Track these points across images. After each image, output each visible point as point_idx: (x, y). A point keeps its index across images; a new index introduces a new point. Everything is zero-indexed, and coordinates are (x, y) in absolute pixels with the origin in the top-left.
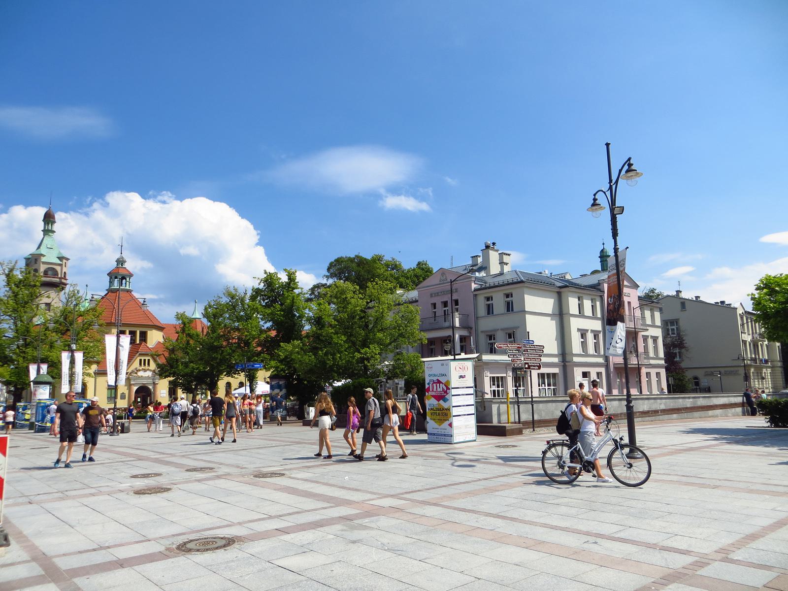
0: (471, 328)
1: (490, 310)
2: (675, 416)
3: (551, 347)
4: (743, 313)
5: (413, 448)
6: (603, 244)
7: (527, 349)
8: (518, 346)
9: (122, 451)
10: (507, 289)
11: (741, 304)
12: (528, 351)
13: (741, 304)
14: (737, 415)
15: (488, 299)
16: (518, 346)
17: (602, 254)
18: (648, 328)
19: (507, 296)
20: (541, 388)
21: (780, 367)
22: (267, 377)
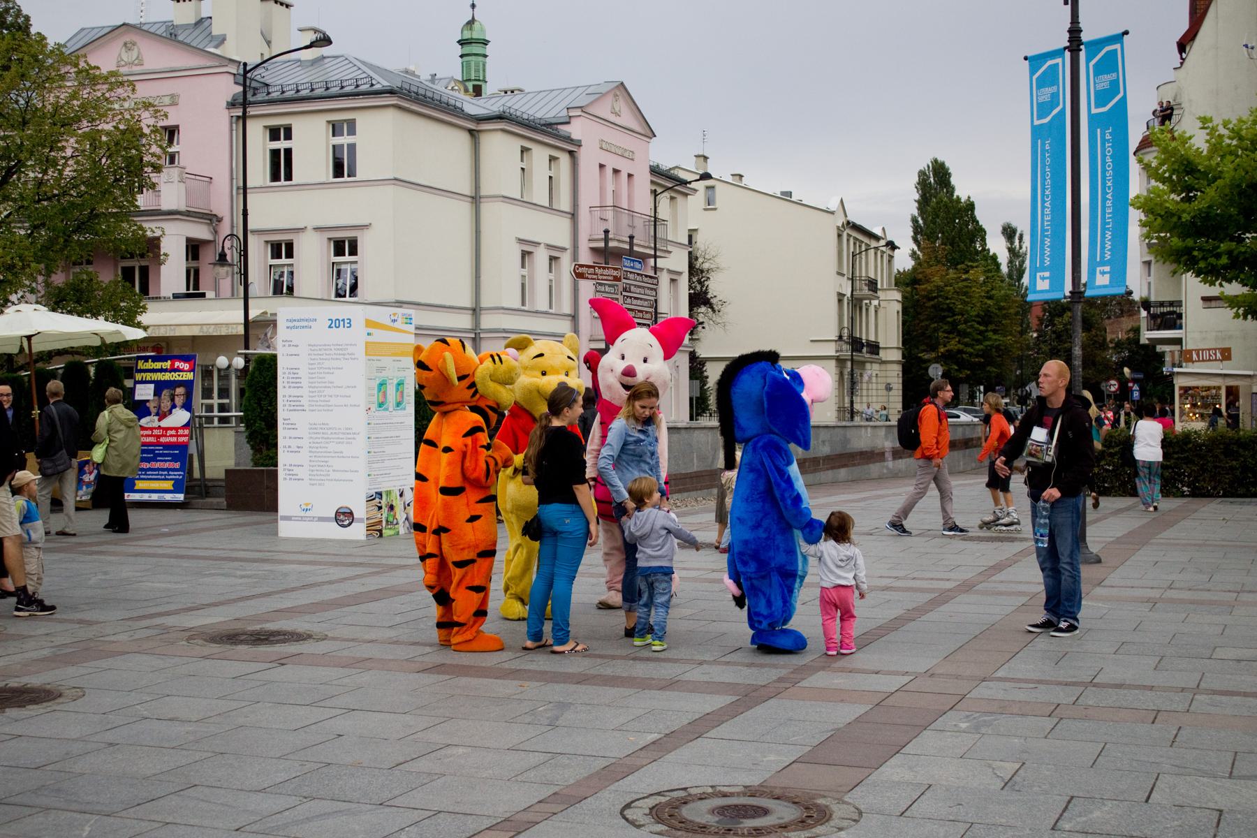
0: (220, 220)
1: (281, 166)
2: (843, 473)
3: (1003, 258)
4: (843, 225)
5: (261, 554)
6: (473, 6)
7: (630, 285)
8: (615, 273)
9: (845, 495)
10: (341, 110)
11: (842, 201)
12: (632, 287)
13: (842, 201)
14: (218, 509)
15: (274, 134)
16: (615, 273)
17: (467, 35)
18: (670, 248)
19: (336, 129)
20: (306, 408)
21: (897, 362)
22: (283, 309)
